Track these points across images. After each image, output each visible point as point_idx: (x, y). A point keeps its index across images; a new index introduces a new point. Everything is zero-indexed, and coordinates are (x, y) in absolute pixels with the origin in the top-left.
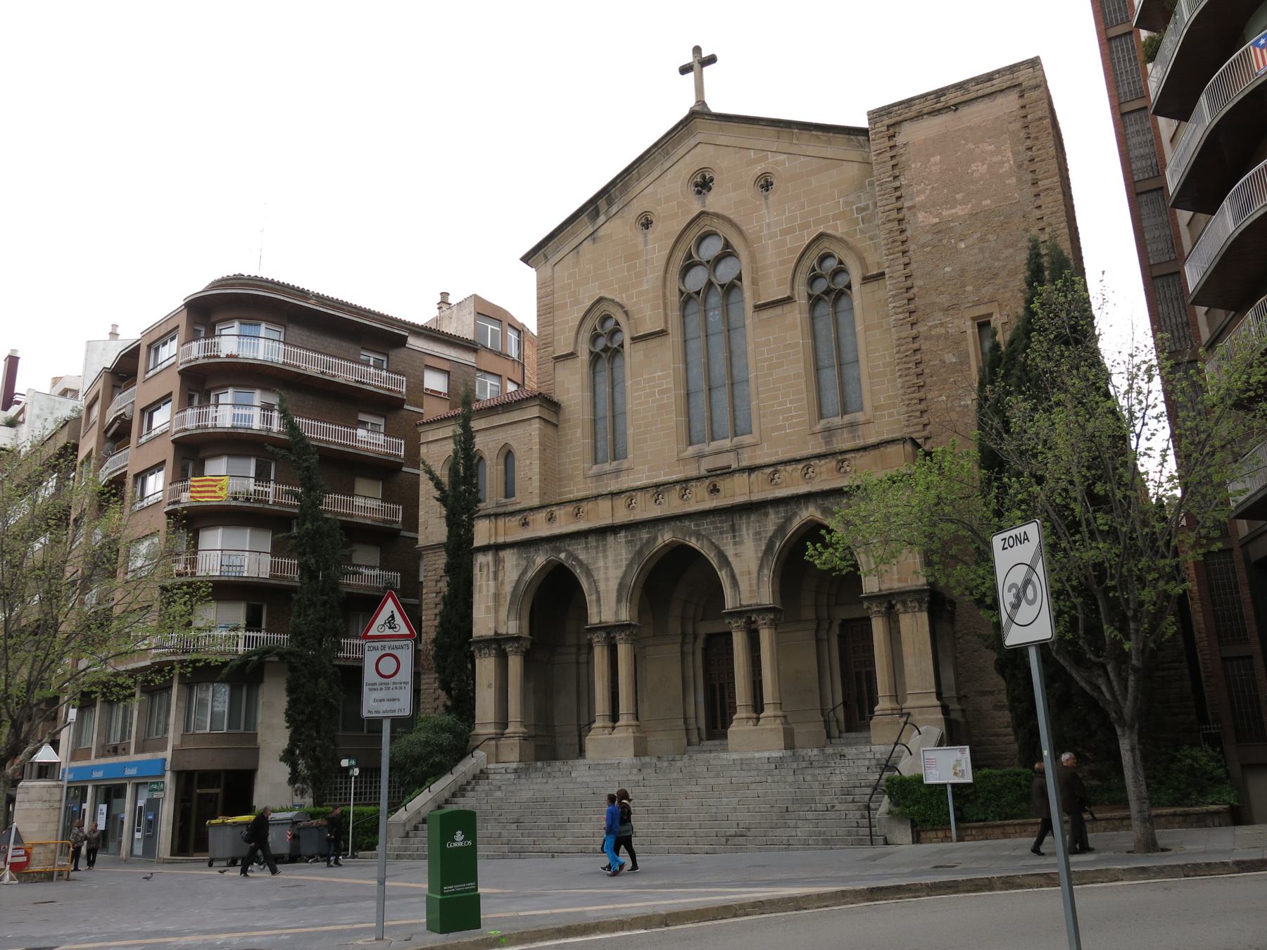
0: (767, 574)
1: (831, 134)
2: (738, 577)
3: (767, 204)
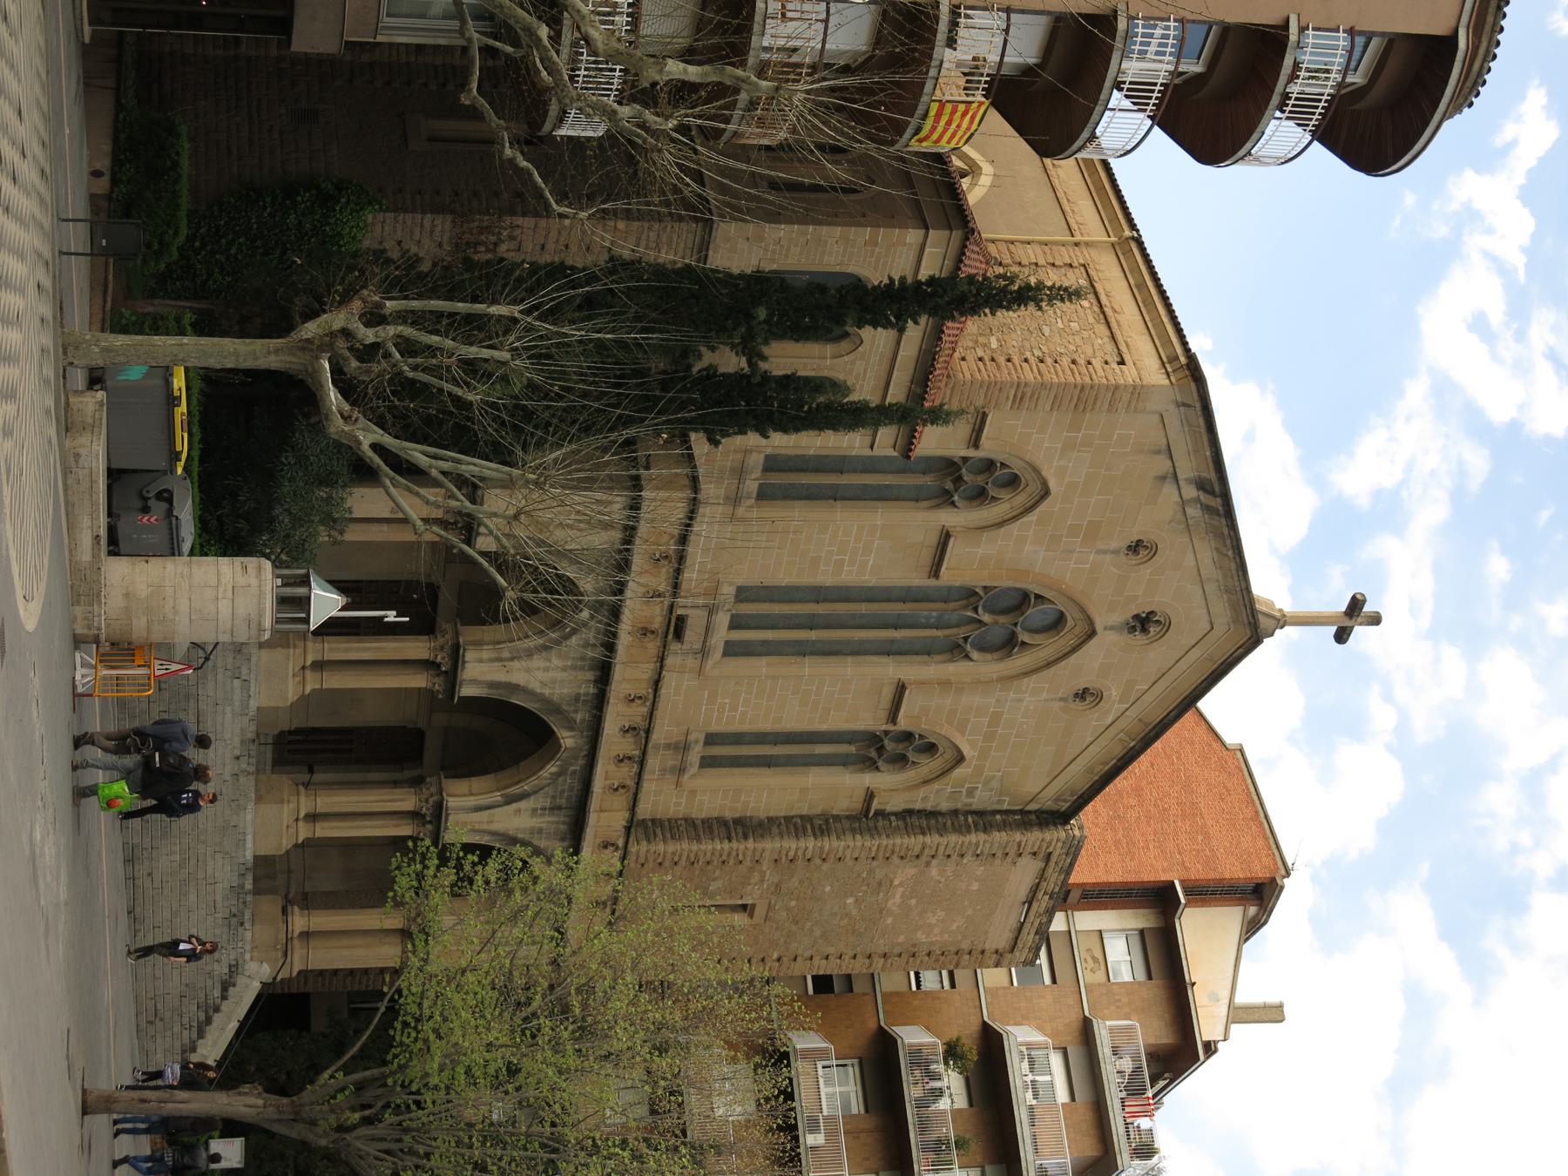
1: (1096, 778)
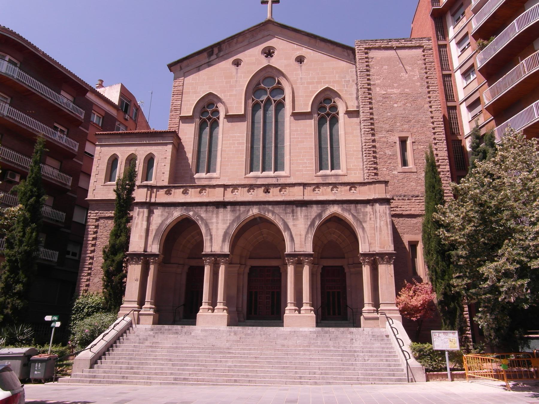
0: (311, 237)
2: (294, 236)
3: (301, 69)
